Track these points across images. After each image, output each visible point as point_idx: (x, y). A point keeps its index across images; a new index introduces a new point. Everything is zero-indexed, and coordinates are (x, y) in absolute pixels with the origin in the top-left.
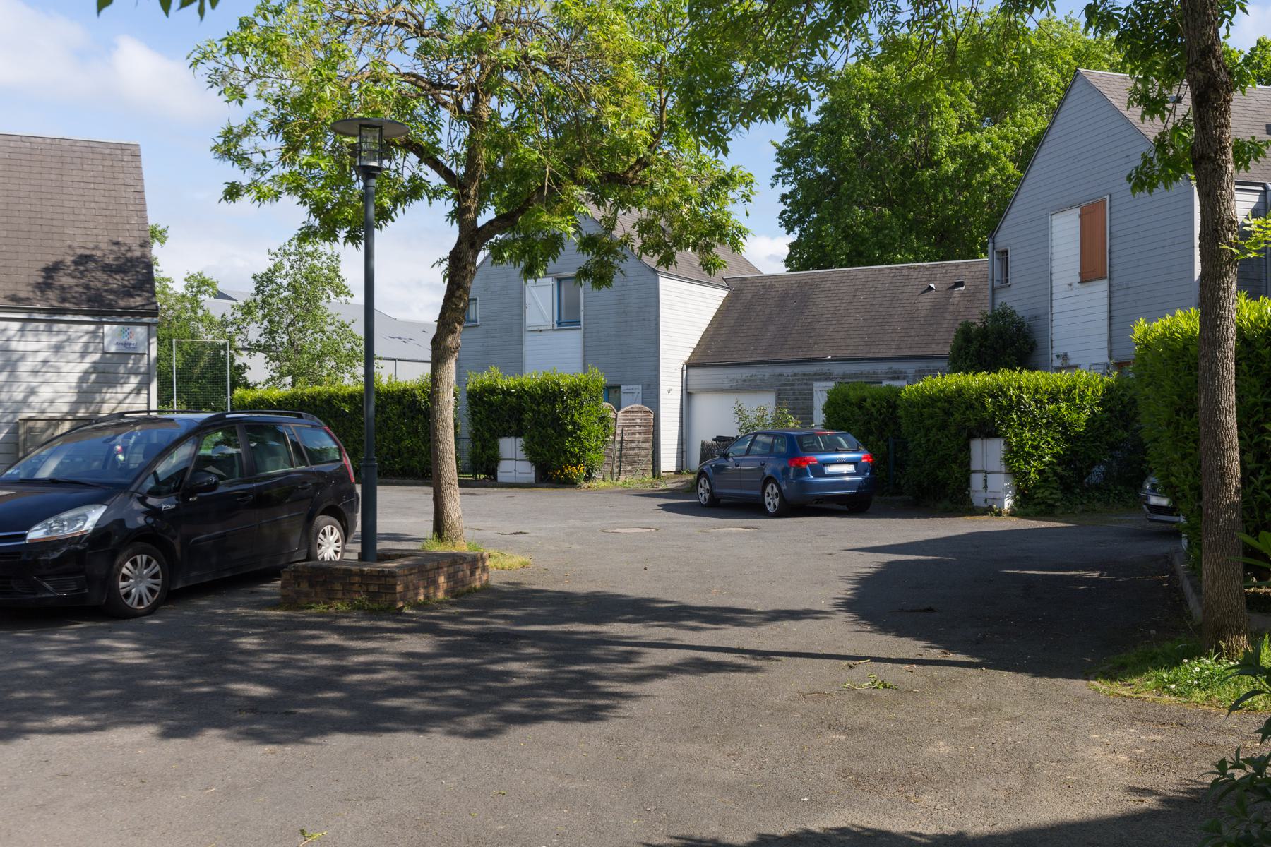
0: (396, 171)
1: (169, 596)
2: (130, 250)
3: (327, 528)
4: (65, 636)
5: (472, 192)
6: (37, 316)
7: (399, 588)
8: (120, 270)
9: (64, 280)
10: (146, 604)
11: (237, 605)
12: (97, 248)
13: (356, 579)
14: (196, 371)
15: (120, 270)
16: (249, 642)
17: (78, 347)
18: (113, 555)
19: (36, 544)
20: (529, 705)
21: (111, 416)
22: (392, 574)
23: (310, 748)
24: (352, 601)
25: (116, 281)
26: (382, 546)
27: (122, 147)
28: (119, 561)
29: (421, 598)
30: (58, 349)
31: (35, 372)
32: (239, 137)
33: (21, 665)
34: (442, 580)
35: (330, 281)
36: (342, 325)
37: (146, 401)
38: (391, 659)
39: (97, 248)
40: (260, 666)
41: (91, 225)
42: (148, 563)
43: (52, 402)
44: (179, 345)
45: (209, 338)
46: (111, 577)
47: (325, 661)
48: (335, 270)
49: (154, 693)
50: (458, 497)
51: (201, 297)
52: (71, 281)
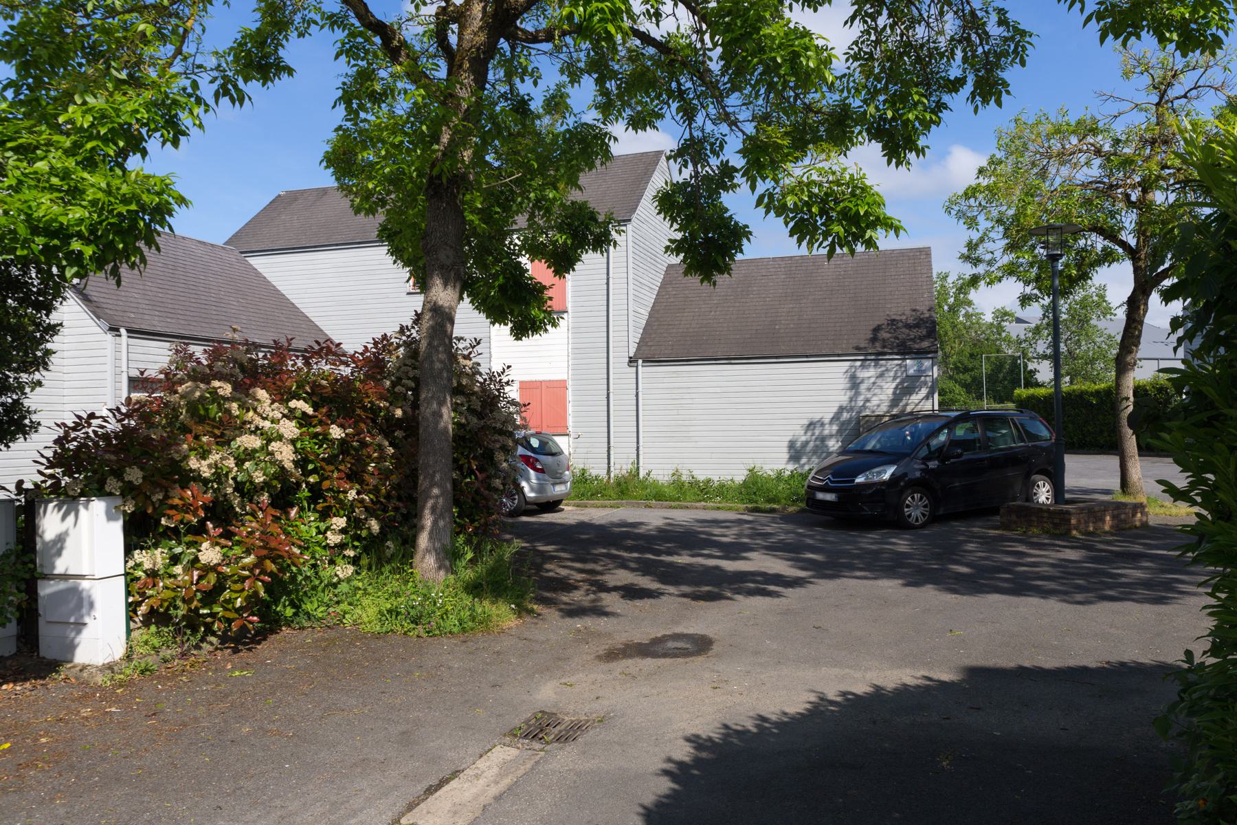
0: (1092, 245)
1: (934, 519)
2: (922, 313)
3: (1040, 483)
4: (874, 536)
5: (1143, 256)
6: (869, 357)
7: (1073, 521)
8: (917, 326)
9: (884, 335)
10: (920, 522)
11: (974, 527)
12: (904, 314)
13: (1046, 515)
14: (1001, 375)
15: (917, 326)
16: (970, 547)
17: (892, 374)
18: (902, 492)
19: (859, 485)
20: (1121, 593)
21: (911, 413)
22: (1068, 513)
23: (976, 598)
24: (1043, 528)
25: (914, 333)
26: (1067, 496)
27: (920, 250)
28: (904, 496)
29: (1091, 529)
30: (881, 375)
31: (869, 389)
32: (977, 245)
33: (848, 547)
34: (1108, 518)
35: (1098, 305)
36: (1109, 336)
37: (931, 405)
38: (1051, 561)
39: (904, 314)
40: (971, 558)
41: (901, 300)
42: (921, 499)
43: (879, 406)
44: (988, 358)
45: (1010, 352)
46: (899, 507)
47: (1010, 559)
48: (1102, 297)
49: (909, 566)
50: (1138, 465)
51: (1004, 324)
52: (888, 335)
